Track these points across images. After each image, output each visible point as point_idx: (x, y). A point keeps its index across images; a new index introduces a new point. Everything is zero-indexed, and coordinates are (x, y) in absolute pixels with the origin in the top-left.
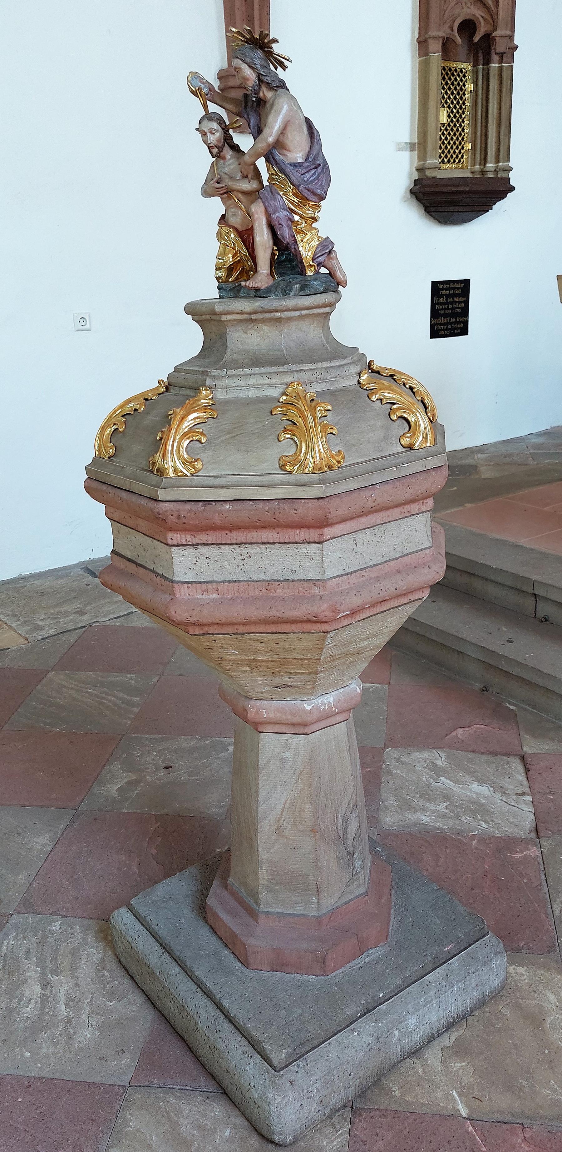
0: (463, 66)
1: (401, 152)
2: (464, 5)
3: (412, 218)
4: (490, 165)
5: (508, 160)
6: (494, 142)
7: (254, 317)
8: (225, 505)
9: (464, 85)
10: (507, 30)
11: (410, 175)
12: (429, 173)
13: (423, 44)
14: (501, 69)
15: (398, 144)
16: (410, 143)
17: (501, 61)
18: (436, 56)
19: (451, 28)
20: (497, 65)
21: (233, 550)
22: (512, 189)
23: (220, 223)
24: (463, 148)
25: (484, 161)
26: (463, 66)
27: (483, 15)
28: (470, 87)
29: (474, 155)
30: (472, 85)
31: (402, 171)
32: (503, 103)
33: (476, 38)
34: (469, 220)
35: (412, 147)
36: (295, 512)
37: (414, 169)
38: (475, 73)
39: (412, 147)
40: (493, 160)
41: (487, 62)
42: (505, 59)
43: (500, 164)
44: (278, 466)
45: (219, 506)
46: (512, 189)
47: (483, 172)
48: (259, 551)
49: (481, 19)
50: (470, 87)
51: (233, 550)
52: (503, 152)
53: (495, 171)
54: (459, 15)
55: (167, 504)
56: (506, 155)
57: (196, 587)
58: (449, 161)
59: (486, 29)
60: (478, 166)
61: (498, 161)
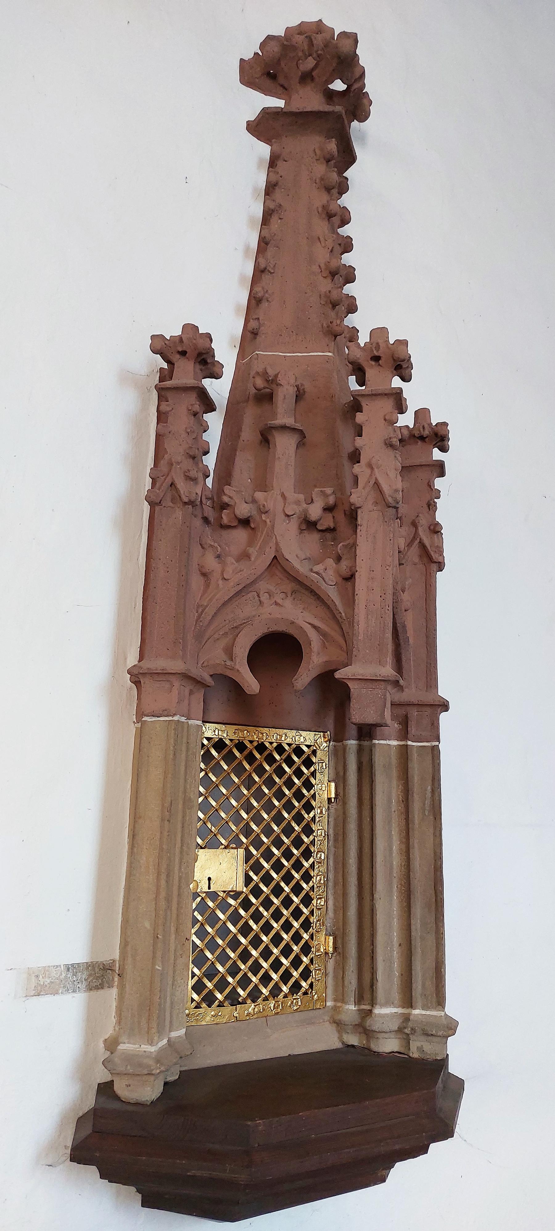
0: (306, 738)
1: (47, 1000)
2: (264, 597)
4: (386, 1012)
5: (440, 1001)
6: (396, 941)
9: (308, 785)
10: (381, 663)
14: (404, 753)
15: (34, 974)
16: (91, 967)
17: (404, 734)
19: (229, 652)
20: (394, 743)
24: (306, 949)
25: (367, 993)
26: (306, 738)
27: (317, 623)
28: (324, 789)
29: (341, 967)
30: (333, 785)
32: (415, 842)
37: (102, 1045)
38: (338, 755)
39: (98, 976)
40: (396, 995)
42: (413, 730)
43: (416, 1012)
49: (313, 635)
50: (324, 789)
52: (425, 977)
53: (400, 1030)
54: (248, 621)
56: (430, 985)
58: (254, 995)
59: (325, 659)
60: (352, 1007)
61: (408, 1002)
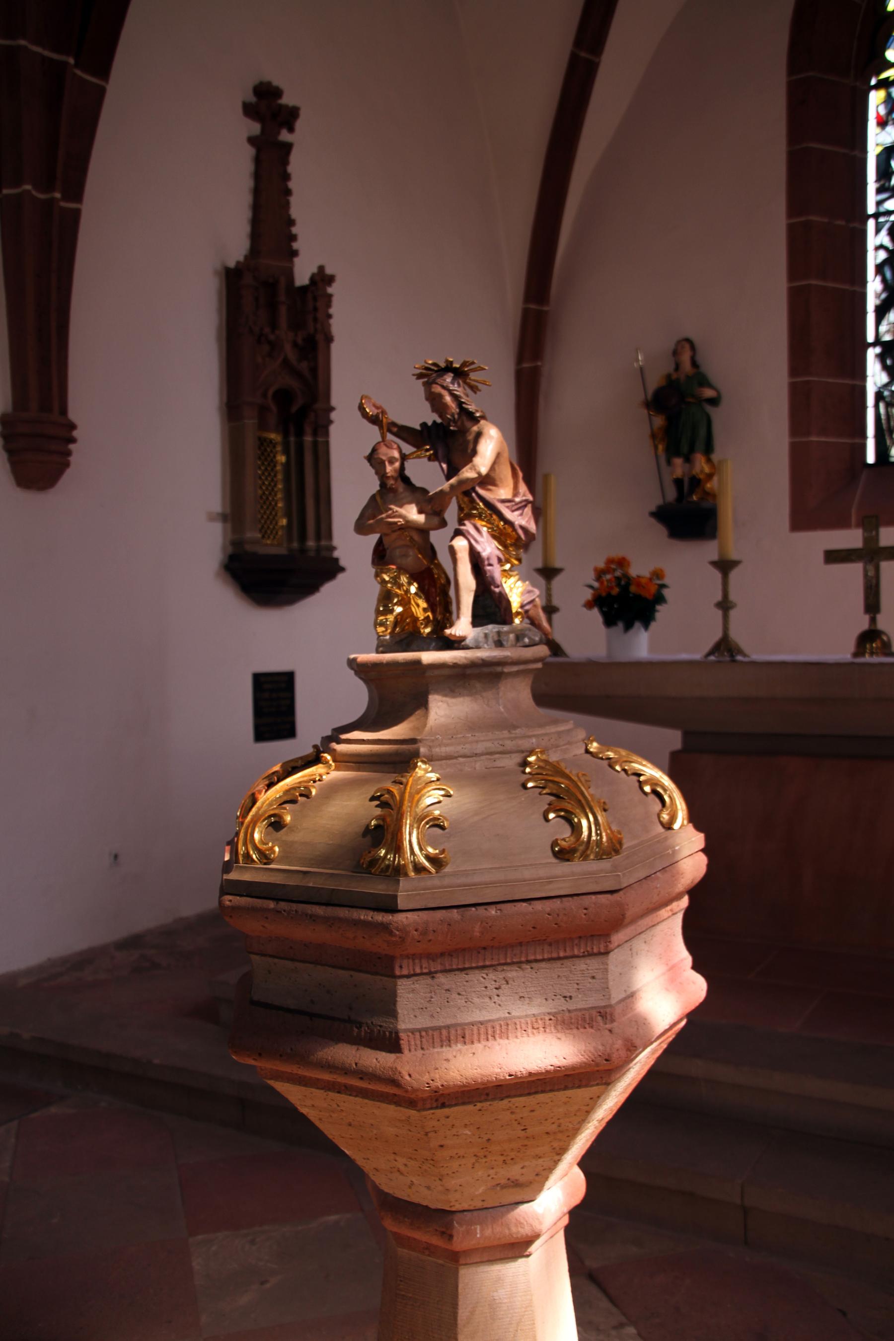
3: (226, 599)
4: (311, 543)
7: (468, 671)
8: (490, 910)
11: (224, 548)
12: (248, 548)
13: (232, 409)
18: (250, 423)
19: (265, 395)
21: (485, 976)
22: (342, 569)
23: (374, 563)
31: (209, 543)
33: (294, 409)
34: (291, 602)
35: (224, 518)
36: (585, 911)
39: (224, 518)
41: (300, 433)
44: (550, 854)
45: (481, 911)
46: (342, 569)
47: (303, 551)
48: (521, 973)
51: (485, 976)
55: (409, 915)
57: (433, 1035)
